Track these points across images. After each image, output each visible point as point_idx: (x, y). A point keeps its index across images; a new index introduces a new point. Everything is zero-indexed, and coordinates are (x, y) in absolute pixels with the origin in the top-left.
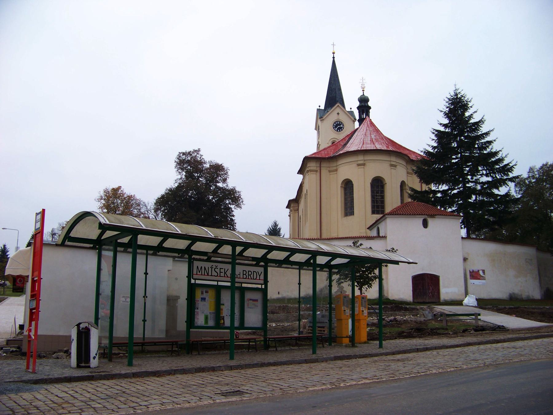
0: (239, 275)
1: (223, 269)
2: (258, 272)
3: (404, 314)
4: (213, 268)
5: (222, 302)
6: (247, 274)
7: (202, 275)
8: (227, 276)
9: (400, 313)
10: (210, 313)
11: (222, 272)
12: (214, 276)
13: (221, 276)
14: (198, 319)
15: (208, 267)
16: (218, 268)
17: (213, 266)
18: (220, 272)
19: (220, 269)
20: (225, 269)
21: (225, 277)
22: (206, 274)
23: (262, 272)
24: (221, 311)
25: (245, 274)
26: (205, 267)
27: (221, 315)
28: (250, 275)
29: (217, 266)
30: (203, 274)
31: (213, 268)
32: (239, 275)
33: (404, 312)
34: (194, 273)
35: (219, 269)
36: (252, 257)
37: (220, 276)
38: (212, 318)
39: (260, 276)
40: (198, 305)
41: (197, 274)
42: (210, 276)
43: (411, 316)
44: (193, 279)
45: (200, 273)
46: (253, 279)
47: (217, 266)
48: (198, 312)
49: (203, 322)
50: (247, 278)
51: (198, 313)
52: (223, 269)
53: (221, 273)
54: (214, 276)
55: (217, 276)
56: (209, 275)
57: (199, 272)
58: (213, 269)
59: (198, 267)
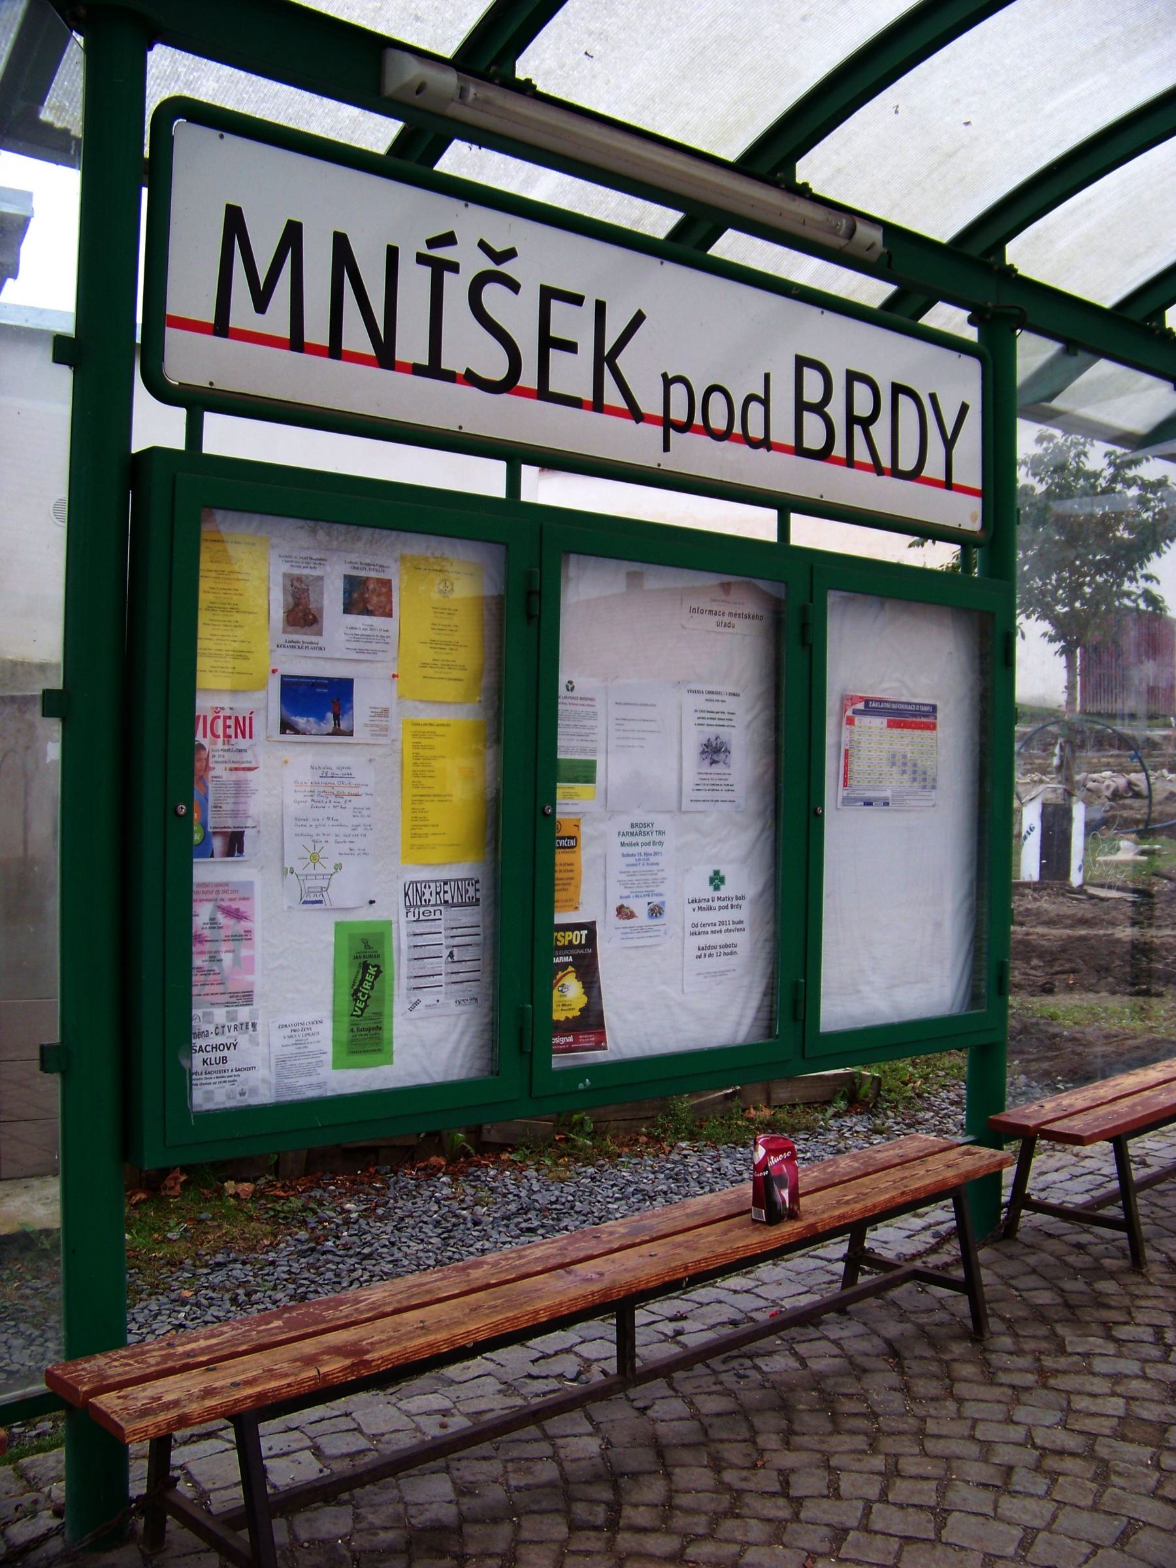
0: (756, 409)
1: (577, 300)
2: (933, 397)
3: (1119, 760)
4: (454, 267)
5: (568, 747)
6: (836, 410)
7: (296, 342)
8: (623, 405)
9: (1103, 756)
10: (415, 896)
11: (570, 347)
12: (471, 379)
13: (554, 387)
14: (246, 997)
15: (392, 254)
16: (514, 286)
17: (448, 239)
18: (547, 342)
19: (548, 294)
20: (600, 307)
21: (598, 405)
22: (356, 338)
23: (964, 408)
24: (561, 857)
25: (818, 409)
26: (341, 243)
27: (560, 918)
28: (866, 423)
29: (511, 254)
30: (317, 331)
31: (454, 267)
32: (756, 409)
33: (1116, 752)
34: (174, 308)
35: (530, 298)
36: (891, 231)
37: (543, 393)
38: (441, 965)
39: (949, 444)
40: (240, 789)
41: (221, 327)
42: (417, 370)
43: (1165, 772)
44: (164, 392)
45: (277, 320)
46: (896, 472)
47: (511, 254)
48: (245, 891)
49: (324, 1037)
50: (839, 450)
51: (237, 915)
52: (577, 300)
53: (554, 353)
54: (471, 379)
55: (508, 385)
56: (401, 356)
57: (261, 301)
58: (456, 288)
59: (234, 220)
